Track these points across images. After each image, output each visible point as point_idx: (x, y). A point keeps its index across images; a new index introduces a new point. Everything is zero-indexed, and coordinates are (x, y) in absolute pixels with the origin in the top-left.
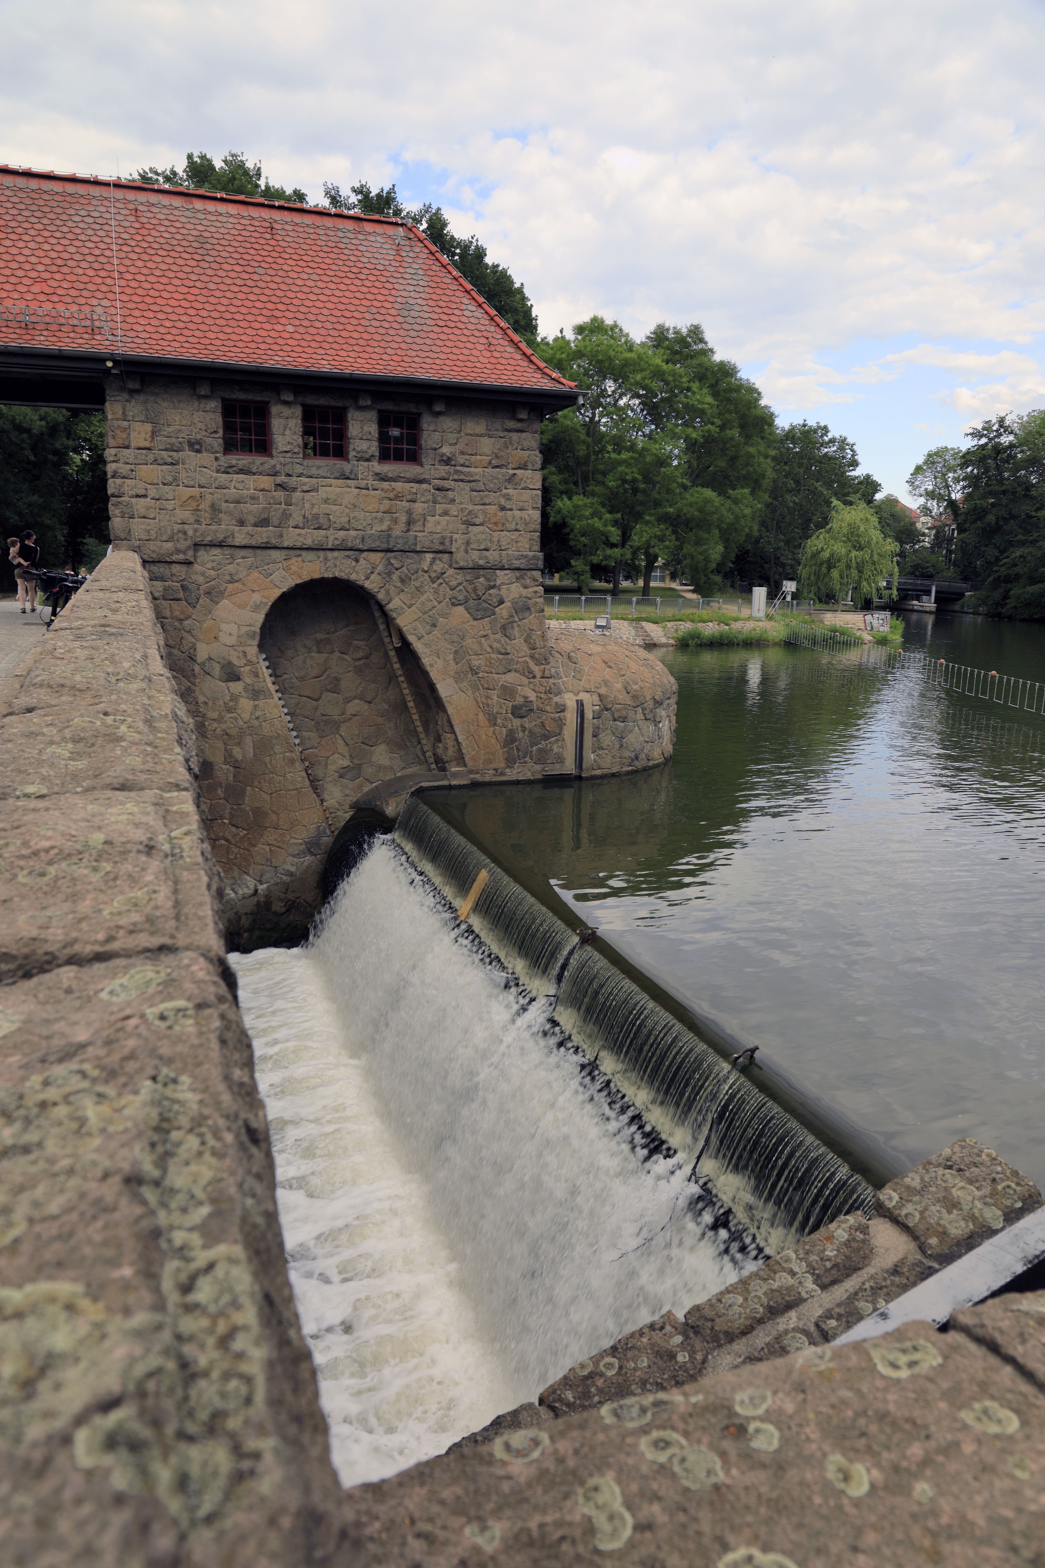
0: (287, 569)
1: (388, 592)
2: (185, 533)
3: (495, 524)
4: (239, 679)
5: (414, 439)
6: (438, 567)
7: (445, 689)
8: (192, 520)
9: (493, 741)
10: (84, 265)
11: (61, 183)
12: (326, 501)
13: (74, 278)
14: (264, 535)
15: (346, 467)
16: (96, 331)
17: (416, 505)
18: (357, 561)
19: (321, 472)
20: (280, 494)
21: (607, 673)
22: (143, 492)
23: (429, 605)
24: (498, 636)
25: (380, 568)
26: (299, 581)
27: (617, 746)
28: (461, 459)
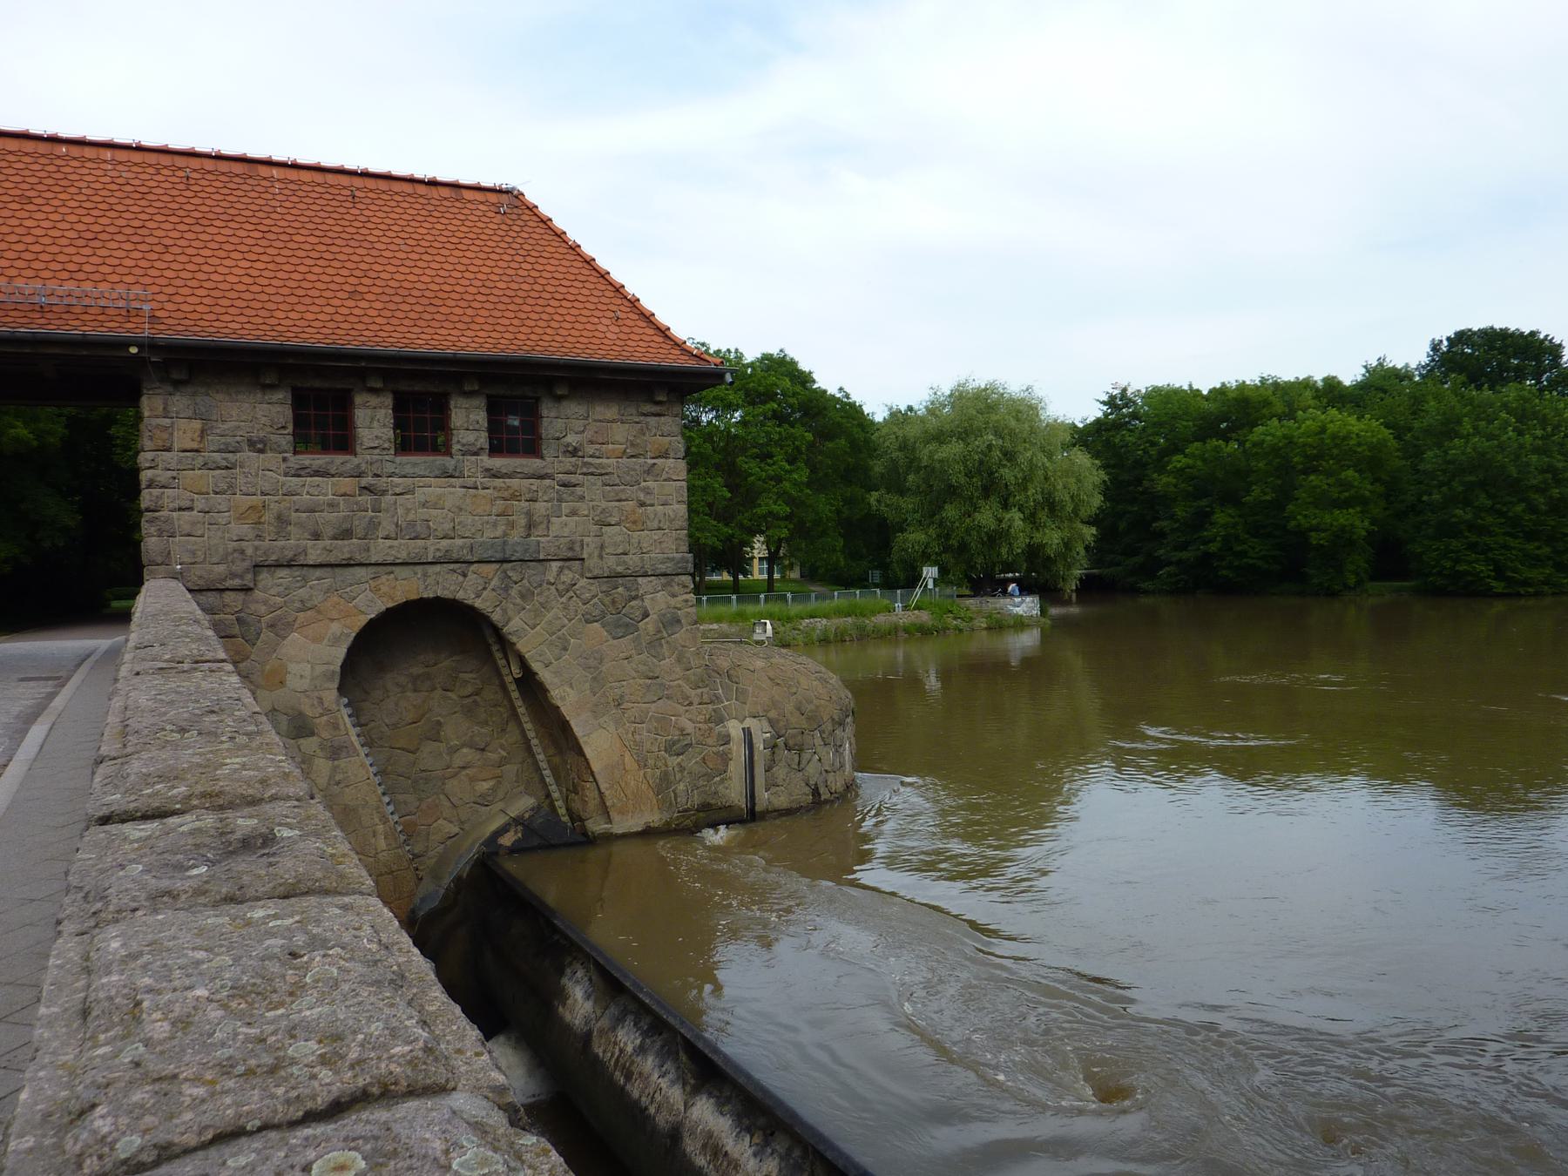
0: (376, 590)
1: (505, 611)
2: (242, 552)
3: (634, 522)
4: (312, 734)
6: (567, 577)
8: (251, 535)
14: (345, 549)
15: (449, 463)
16: (133, 313)
17: (537, 505)
18: (465, 575)
20: (367, 499)
22: (187, 504)
25: (495, 582)
26: (390, 605)
28: (590, 449)
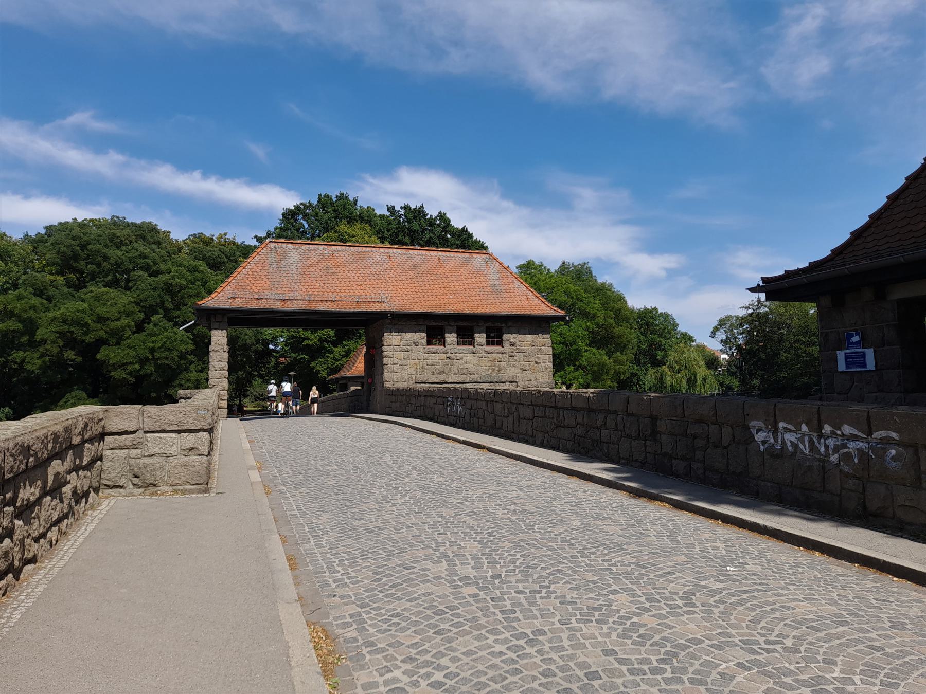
5: (500, 337)
12: (466, 363)
20: (448, 361)
28: (519, 344)
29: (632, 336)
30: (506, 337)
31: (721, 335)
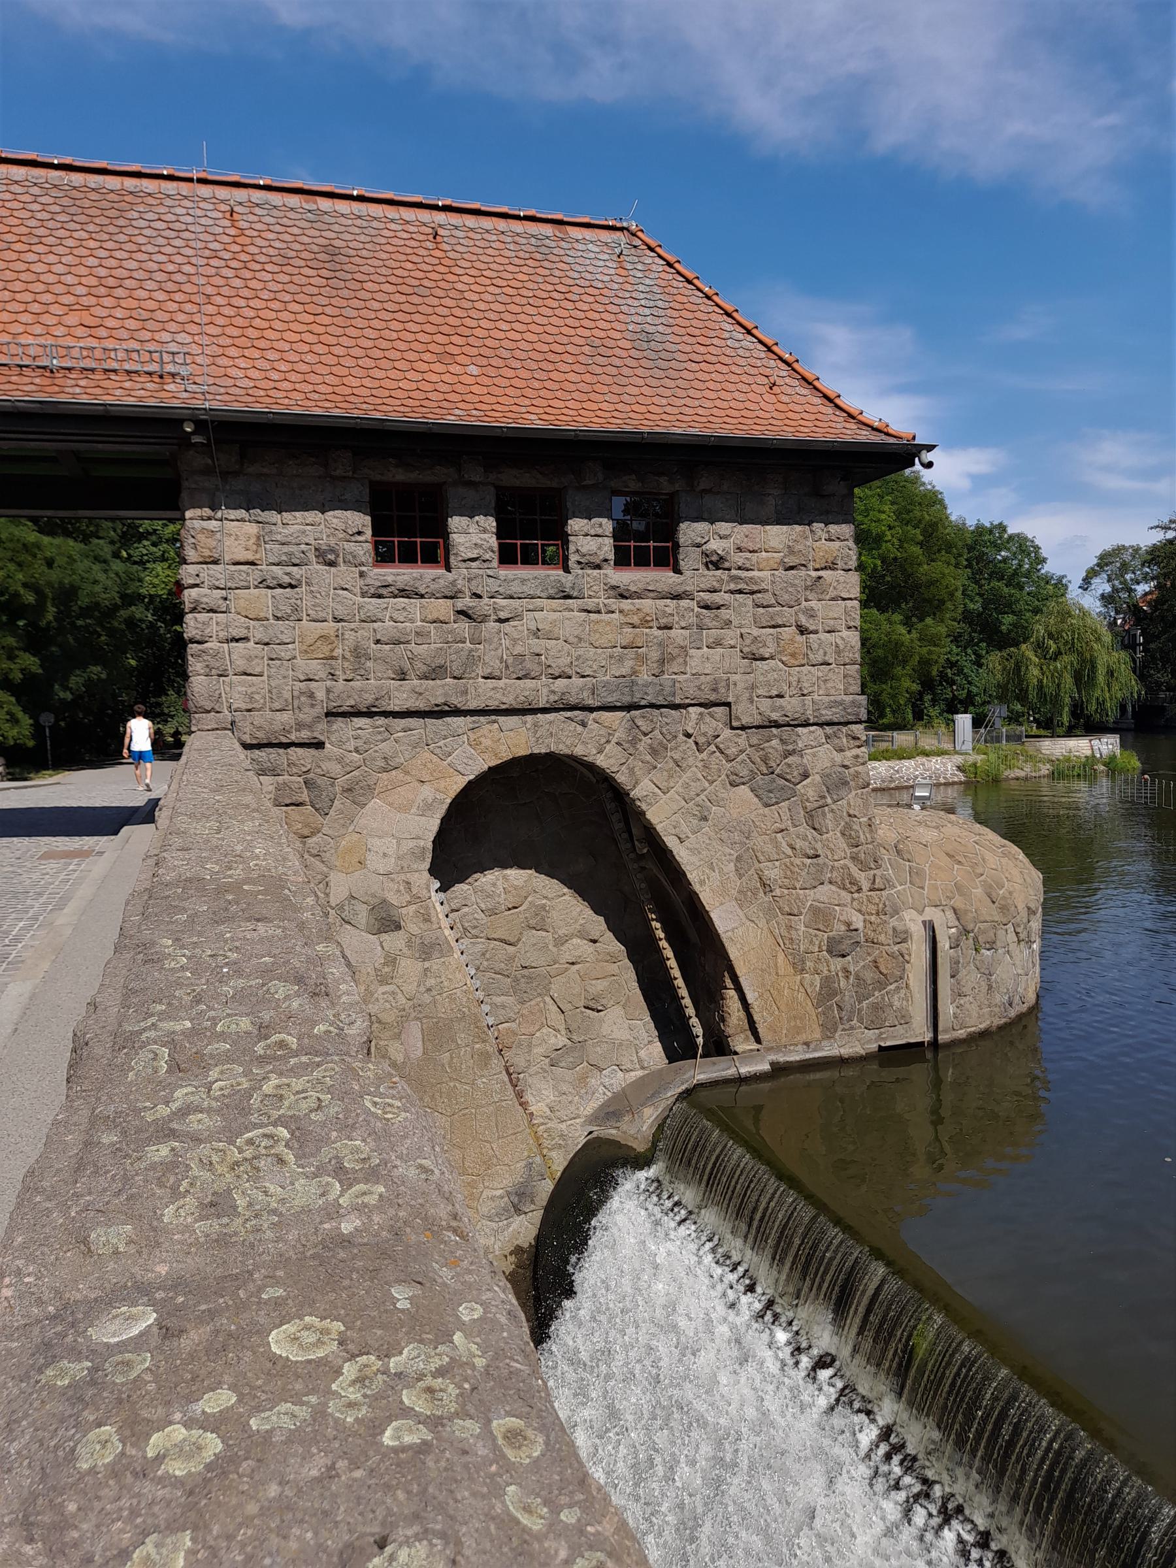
0: (475, 744)
1: (632, 770)
2: (311, 695)
3: (793, 655)
5: (669, 533)
7: (724, 918)
9: (801, 996)
10: (150, 285)
11: (119, 179)
12: (536, 633)
13: (135, 304)
14: (439, 692)
17: (673, 633)
18: (584, 724)
19: (528, 589)
20: (464, 626)
21: (959, 873)
22: (241, 633)
23: (695, 787)
24: (801, 829)
26: (493, 763)
27: (985, 988)
28: (739, 559)
29: (956, 579)
30: (690, 532)
31: (1102, 586)
